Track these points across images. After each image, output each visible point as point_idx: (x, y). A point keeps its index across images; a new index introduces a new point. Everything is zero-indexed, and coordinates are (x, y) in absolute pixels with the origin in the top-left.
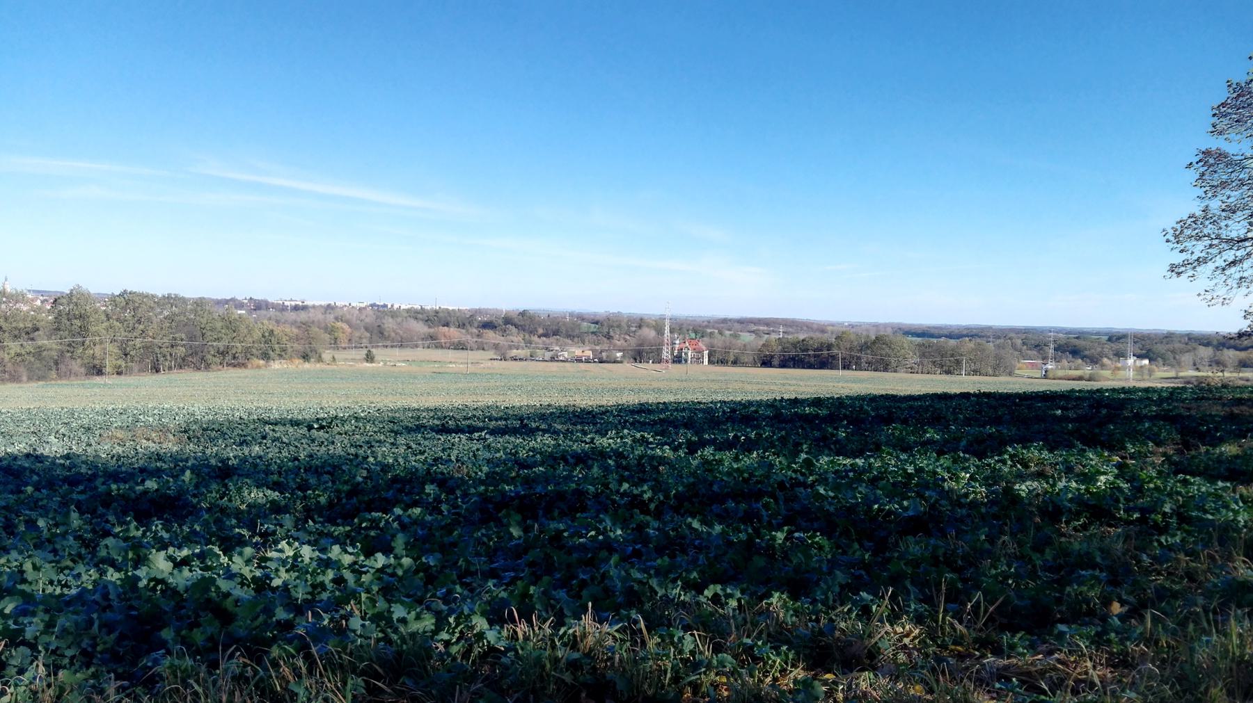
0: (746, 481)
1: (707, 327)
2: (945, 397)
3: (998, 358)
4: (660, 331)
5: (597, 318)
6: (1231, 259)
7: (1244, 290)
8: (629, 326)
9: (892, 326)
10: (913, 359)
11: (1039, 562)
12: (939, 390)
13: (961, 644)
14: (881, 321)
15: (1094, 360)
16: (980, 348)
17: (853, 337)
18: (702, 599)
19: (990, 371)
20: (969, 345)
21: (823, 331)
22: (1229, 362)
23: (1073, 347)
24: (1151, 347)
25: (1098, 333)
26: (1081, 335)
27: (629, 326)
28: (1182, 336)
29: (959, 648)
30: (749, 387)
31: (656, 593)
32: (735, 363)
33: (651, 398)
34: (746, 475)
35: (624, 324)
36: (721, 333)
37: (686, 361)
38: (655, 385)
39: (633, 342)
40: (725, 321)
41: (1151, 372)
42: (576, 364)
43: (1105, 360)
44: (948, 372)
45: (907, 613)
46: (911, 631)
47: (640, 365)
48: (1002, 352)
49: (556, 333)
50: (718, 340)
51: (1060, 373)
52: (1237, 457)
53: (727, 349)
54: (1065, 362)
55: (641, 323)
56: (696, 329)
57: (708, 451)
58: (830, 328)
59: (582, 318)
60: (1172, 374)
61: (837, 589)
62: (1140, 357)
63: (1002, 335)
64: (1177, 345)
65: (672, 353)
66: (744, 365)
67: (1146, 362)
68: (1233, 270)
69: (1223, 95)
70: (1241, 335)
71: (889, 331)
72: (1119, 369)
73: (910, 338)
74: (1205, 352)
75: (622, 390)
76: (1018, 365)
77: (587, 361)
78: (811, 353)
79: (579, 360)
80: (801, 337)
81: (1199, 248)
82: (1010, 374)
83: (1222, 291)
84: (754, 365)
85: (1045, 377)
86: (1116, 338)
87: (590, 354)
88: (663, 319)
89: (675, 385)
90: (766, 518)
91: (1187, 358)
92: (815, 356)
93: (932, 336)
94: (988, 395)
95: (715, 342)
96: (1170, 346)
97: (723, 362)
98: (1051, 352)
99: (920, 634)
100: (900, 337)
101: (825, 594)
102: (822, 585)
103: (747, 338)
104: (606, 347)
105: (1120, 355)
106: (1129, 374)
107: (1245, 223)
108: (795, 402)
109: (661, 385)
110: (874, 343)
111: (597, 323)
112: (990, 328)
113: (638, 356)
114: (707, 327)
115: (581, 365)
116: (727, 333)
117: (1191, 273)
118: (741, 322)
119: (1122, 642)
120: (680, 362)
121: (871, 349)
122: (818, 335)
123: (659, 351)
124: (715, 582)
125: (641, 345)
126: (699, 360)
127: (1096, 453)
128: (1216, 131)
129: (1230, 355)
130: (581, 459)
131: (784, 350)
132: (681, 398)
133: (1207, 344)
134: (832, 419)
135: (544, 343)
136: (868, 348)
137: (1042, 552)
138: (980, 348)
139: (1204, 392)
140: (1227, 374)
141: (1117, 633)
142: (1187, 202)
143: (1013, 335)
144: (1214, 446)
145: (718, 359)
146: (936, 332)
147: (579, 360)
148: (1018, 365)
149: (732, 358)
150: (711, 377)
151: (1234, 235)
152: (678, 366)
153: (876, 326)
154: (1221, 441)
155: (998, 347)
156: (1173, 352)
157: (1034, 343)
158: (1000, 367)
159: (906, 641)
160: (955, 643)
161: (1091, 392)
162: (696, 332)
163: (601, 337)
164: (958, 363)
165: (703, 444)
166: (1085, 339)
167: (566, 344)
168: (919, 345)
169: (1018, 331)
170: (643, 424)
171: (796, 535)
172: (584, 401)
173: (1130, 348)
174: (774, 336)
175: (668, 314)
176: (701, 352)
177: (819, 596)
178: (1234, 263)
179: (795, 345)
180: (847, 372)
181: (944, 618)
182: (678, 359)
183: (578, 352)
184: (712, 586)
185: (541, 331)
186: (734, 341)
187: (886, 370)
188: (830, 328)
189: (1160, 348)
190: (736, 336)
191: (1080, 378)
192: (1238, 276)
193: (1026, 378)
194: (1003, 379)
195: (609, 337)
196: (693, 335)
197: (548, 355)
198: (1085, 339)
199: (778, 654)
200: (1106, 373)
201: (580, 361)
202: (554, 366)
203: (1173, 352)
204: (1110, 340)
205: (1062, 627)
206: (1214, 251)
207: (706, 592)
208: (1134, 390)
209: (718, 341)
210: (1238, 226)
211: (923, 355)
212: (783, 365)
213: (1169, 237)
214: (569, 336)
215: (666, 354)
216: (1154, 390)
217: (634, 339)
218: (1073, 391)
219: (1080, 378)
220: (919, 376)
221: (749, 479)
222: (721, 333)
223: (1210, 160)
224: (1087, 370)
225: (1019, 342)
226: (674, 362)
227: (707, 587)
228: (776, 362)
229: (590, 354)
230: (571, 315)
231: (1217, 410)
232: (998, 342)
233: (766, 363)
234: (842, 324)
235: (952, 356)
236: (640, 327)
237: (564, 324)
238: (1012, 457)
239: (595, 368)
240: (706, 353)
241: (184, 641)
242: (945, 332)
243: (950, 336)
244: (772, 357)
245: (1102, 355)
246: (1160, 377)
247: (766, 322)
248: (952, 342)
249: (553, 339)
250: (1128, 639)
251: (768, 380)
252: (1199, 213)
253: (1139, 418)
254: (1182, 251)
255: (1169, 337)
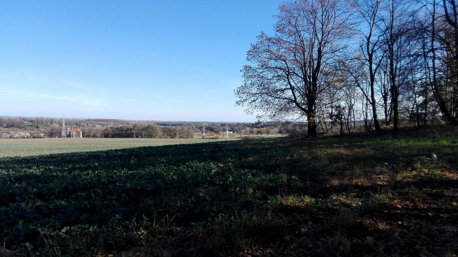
0: (89, 183)
1: (81, 123)
2: (170, 146)
3: (188, 132)
4: (61, 125)
5: (32, 119)
6: (253, 100)
7: (256, 109)
8: (47, 123)
9: (153, 122)
10: (161, 134)
11: (190, 202)
12: (168, 144)
13: (161, 235)
14: (149, 120)
15: (217, 132)
16: (182, 129)
17: (139, 126)
18: (61, 233)
19: (186, 137)
20: (179, 128)
21: (128, 124)
22: (255, 132)
23: (211, 128)
24: (234, 128)
25: (218, 124)
26: (213, 124)
27: (47, 123)
28: (242, 124)
29: (160, 236)
30: (99, 146)
31: (40, 234)
32: (94, 136)
33: (56, 152)
34: (89, 181)
35: (44, 122)
36: (87, 125)
37: (72, 136)
38: (59, 146)
39: (48, 129)
40: (89, 120)
41: (233, 136)
42: (22, 139)
43: (220, 132)
44: (172, 138)
45: (142, 226)
46: (144, 233)
47: (51, 139)
48: (189, 130)
49: (12, 126)
50: (87, 128)
51: (207, 137)
52: (253, 161)
53: (90, 131)
54: (208, 133)
55: (52, 121)
56: (77, 124)
57: (77, 172)
58: (131, 123)
59: (24, 119)
60: (239, 136)
61: (116, 221)
62: (230, 131)
63: (189, 124)
64: (240, 127)
65: (66, 133)
66: (97, 137)
67: (232, 132)
68: (253, 103)
69: (249, 48)
70: (256, 124)
71: (152, 124)
72: (224, 135)
73: (159, 126)
74: (248, 129)
75: (43, 149)
76: (194, 135)
77: (27, 138)
78: (124, 132)
79: (24, 137)
80: (120, 126)
81: (244, 96)
82: (192, 138)
83: (250, 110)
84: (101, 137)
85: (203, 138)
86: (223, 125)
87: (29, 135)
88: (62, 120)
89: (67, 146)
90: (94, 197)
91: (243, 131)
92: (125, 133)
93: (167, 125)
94: (183, 145)
95: (85, 128)
96: (238, 127)
97: (88, 136)
98: (204, 130)
99: (147, 233)
100: (156, 126)
101: (112, 223)
102: (111, 220)
103: (98, 127)
104: (36, 131)
105: (224, 130)
106: (227, 136)
107: (256, 89)
108: (116, 150)
109: (61, 146)
110: (147, 128)
111: (32, 121)
112: (185, 122)
113: (51, 135)
114: (81, 123)
115: (24, 139)
116: (90, 125)
117: (242, 104)
118: (95, 120)
119: (212, 225)
120: (70, 137)
121: (147, 130)
122: (126, 125)
123: (60, 133)
124: (66, 226)
125: (52, 130)
126: (78, 136)
127: (214, 164)
128: (248, 59)
129: (255, 130)
130: (18, 179)
131: (113, 131)
132: (70, 151)
133: (249, 126)
134: (129, 157)
135: (6, 130)
136: (145, 130)
137: (191, 198)
138: (182, 129)
139: (246, 141)
140: (254, 136)
141: (210, 223)
142: (240, 82)
143: (192, 124)
144: (247, 158)
145: (86, 135)
146: (168, 124)
147: (24, 137)
148: (194, 135)
149: (92, 135)
150: (84, 142)
151: (253, 92)
152: (69, 138)
153: (148, 122)
154: (249, 156)
155: (188, 129)
156: (239, 129)
157: (199, 127)
158: (189, 135)
159: (142, 237)
160: (159, 235)
161: (215, 143)
162: (76, 125)
163: (34, 128)
164: (175, 134)
165: (76, 169)
166: (214, 125)
167: (17, 131)
168: (163, 129)
169: (194, 123)
170: (50, 162)
171: (105, 202)
172: (23, 154)
173: (227, 128)
174: (109, 126)
175: (64, 117)
176: (79, 133)
177: (110, 225)
178: (254, 101)
179: (117, 129)
180: (137, 139)
181: (155, 226)
182: (69, 136)
183: (23, 134)
184: (65, 228)
185: (5, 125)
186: (93, 128)
187: (151, 137)
188: (131, 123)
189: (236, 128)
190: (94, 126)
191: (213, 138)
192: (255, 105)
193: (197, 138)
194: (190, 139)
195: (37, 127)
196: (75, 126)
197: (8, 135)
198: (214, 125)
199: (90, 251)
200: (220, 136)
201: (24, 138)
202: (11, 140)
203: (239, 129)
204: (221, 125)
205: (193, 223)
206: (248, 97)
207: (63, 230)
208: (227, 141)
209: (86, 128)
210: (253, 90)
211: (164, 132)
212: (113, 136)
213: (236, 92)
214: (20, 128)
215: (63, 133)
216: (232, 141)
217: (52, 128)
218: (210, 142)
219: (213, 138)
220: (163, 139)
221: (91, 182)
222: (87, 125)
223: (247, 68)
224: (215, 135)
225: (195, 127)
226: (67, 137)
227: (63, 228)
228: (110, 136)
229: (29, 135)
230: (19, 118)
231: (249, 147)
232: (188, 127)
233: (106, 136)
234: (135, 121)
235: (173, 132)
236: (52, 123)
237: (16, 122)
238: (187, 166)
239: (31, 140)
240: (81, 133)
241: (398, 240)
242: (171, 124)
243: (173, 125)
244: (109, 134)
245: (219, 130)
246: (236, 137)
247: (107, 121)
248: (173, 127)
249: (11, 129)
250: (214, 224)
251: (107, 143)
252: (244, 85)
253: (227, 150)
254: (239, 97)
255: (238, 124)
